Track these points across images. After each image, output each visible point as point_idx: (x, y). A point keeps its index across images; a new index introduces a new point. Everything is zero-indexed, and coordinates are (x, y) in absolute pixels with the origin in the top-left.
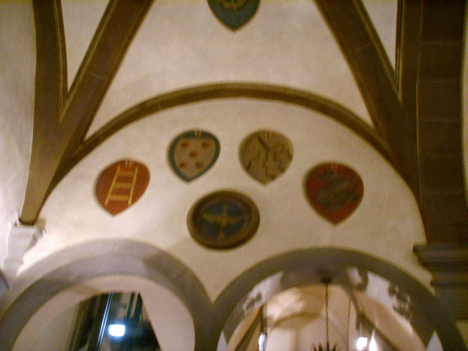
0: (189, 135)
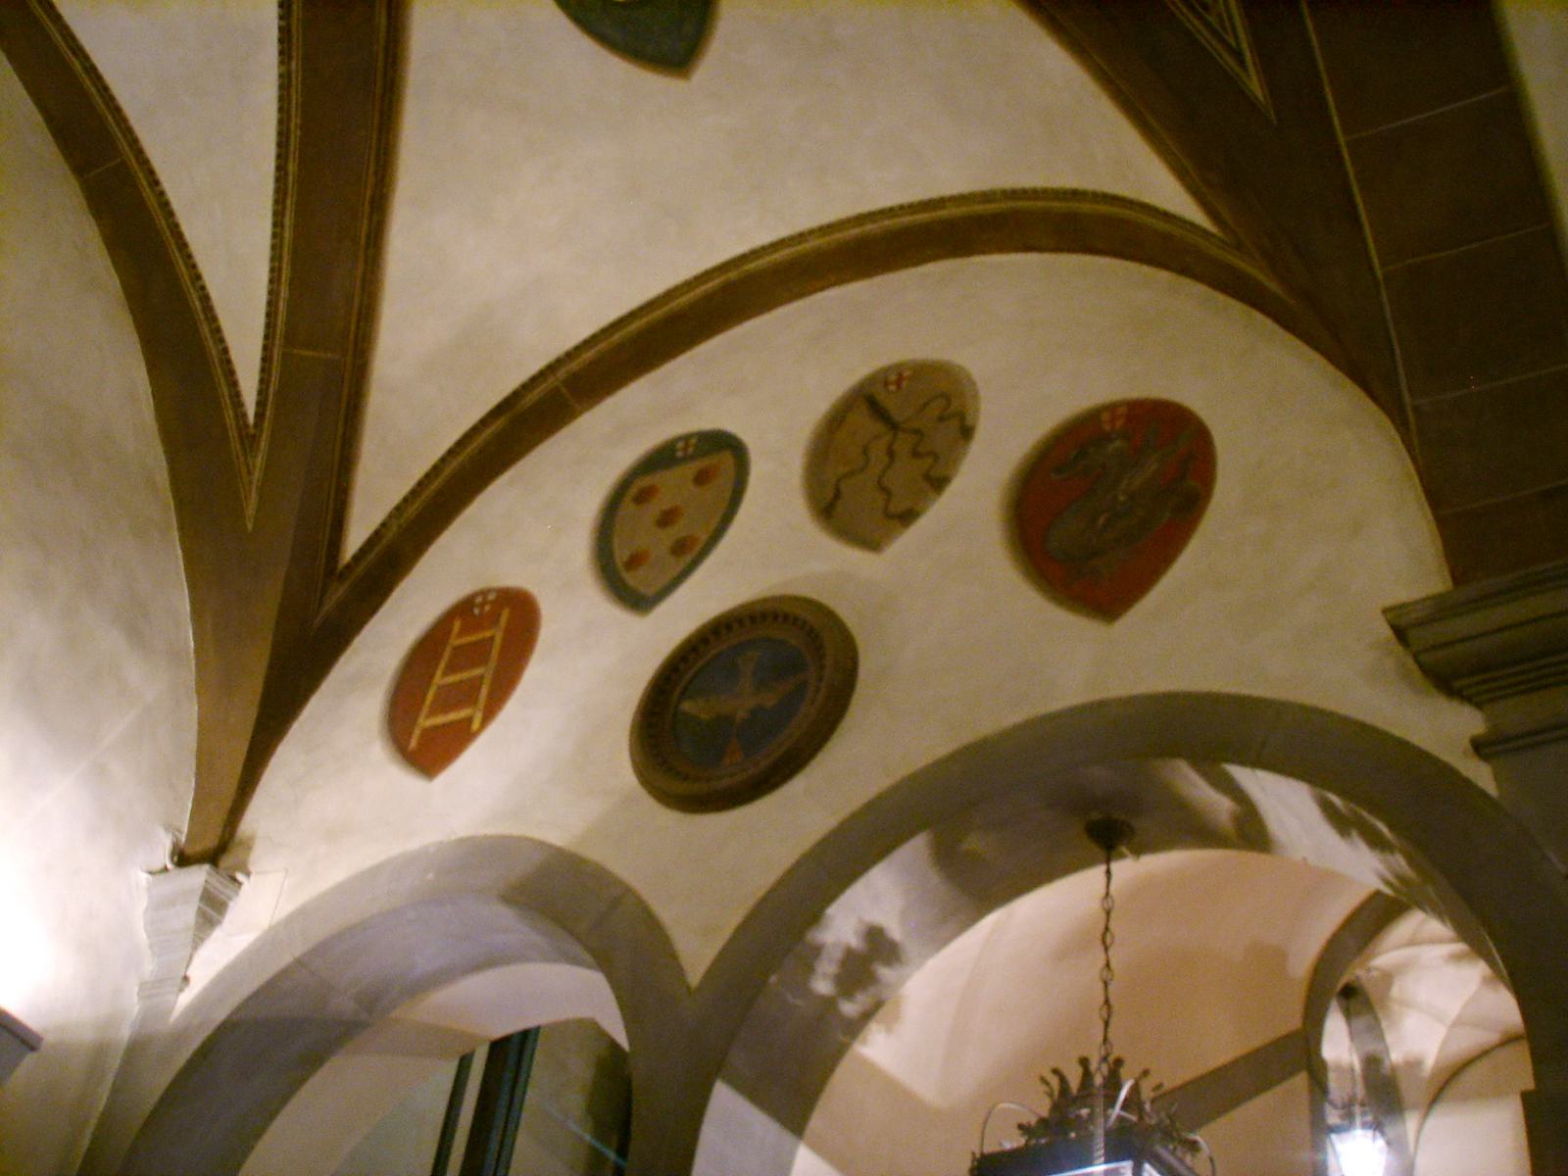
0: (661, 459)
